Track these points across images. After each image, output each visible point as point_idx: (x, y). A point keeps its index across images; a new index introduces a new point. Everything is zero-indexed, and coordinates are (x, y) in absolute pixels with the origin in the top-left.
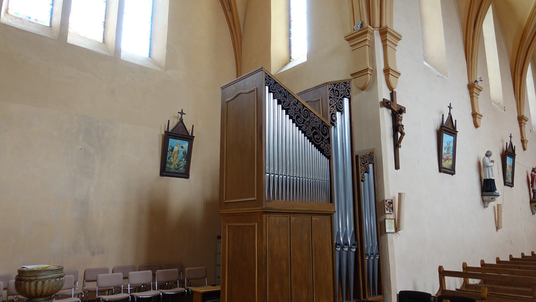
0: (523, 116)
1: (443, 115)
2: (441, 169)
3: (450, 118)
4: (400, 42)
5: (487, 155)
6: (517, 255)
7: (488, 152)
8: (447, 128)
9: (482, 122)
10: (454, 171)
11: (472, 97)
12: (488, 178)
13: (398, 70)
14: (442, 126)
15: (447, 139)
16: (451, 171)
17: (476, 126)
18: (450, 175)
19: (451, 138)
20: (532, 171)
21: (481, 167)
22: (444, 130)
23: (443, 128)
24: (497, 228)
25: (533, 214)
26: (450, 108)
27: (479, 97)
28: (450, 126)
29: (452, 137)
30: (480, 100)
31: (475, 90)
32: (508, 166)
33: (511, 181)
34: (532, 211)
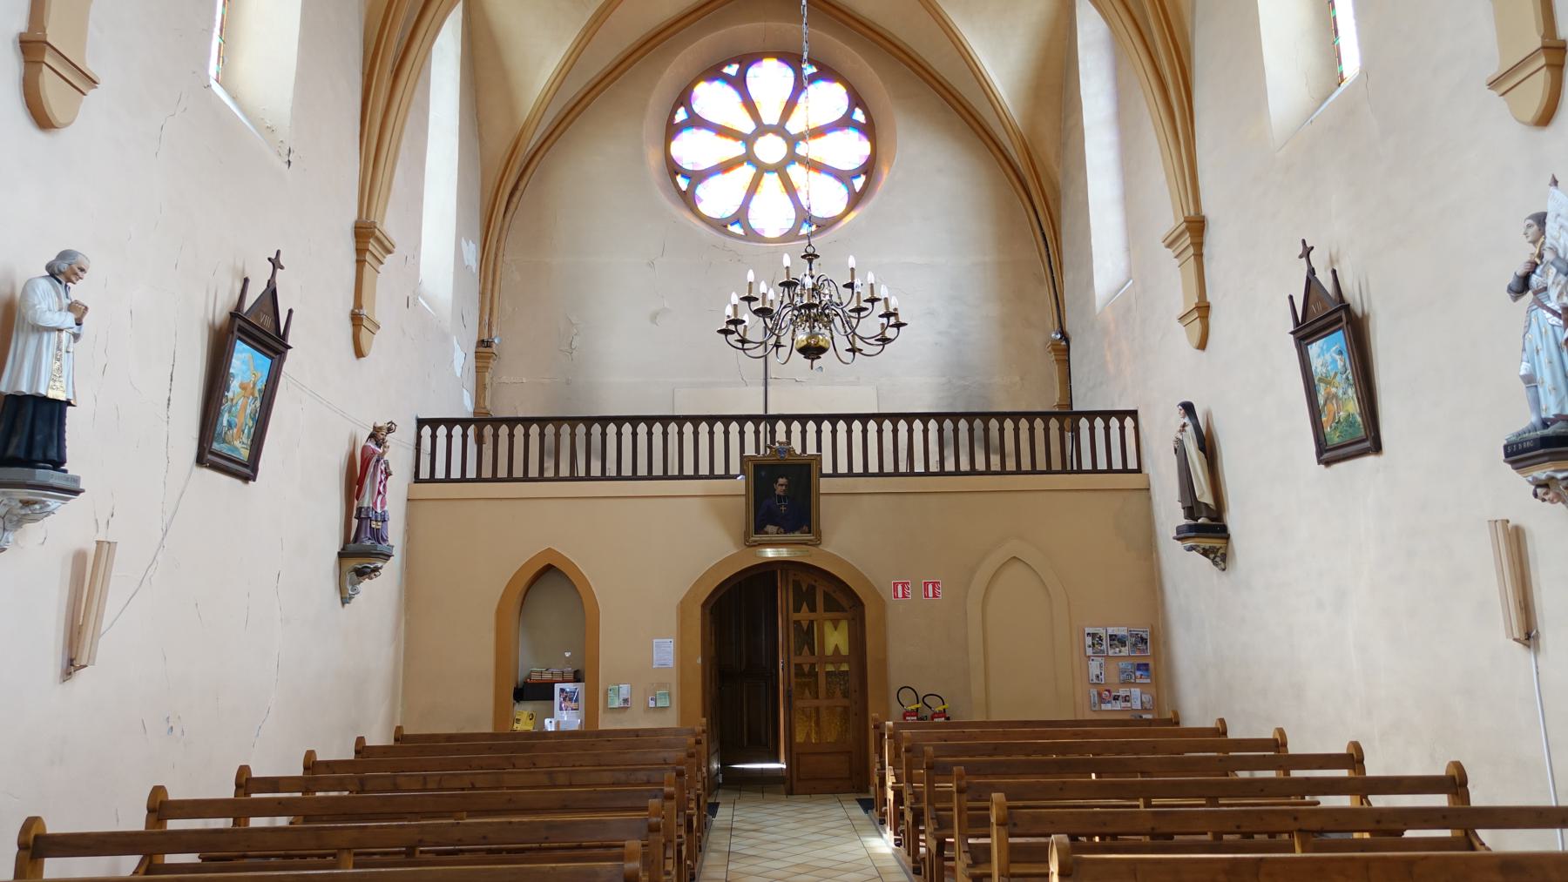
0: (373, 226)
1: (246, 280)
2: (207, 456)
3: (271, 293)
4: (389, 256)
5: (53, 273)
6: (338, 749)
7: (64, 255)
8: (255, 327)
9: (377, 345)
10: (255, 469)
11: (360, 262)
12: (24, 388)
13: (90, 67)
14: (235, 315)
15: (245, 363)
16: (246, 471)
17: (359, 353)
18: (238, 482)
19: (265, 363)
20: (372, 436)
21: (360, 473)
22: (241, 330)
23: (238, 322)
24: (71, 666)
25: (345, 600)
26: (276, 263)
27: (381, 268)
28: (266, 322)
29: (269, 361)
30: (386, 279)
31: (373, 246)
32: (235, 385)
33: (244, 454)
34: (342, 589)
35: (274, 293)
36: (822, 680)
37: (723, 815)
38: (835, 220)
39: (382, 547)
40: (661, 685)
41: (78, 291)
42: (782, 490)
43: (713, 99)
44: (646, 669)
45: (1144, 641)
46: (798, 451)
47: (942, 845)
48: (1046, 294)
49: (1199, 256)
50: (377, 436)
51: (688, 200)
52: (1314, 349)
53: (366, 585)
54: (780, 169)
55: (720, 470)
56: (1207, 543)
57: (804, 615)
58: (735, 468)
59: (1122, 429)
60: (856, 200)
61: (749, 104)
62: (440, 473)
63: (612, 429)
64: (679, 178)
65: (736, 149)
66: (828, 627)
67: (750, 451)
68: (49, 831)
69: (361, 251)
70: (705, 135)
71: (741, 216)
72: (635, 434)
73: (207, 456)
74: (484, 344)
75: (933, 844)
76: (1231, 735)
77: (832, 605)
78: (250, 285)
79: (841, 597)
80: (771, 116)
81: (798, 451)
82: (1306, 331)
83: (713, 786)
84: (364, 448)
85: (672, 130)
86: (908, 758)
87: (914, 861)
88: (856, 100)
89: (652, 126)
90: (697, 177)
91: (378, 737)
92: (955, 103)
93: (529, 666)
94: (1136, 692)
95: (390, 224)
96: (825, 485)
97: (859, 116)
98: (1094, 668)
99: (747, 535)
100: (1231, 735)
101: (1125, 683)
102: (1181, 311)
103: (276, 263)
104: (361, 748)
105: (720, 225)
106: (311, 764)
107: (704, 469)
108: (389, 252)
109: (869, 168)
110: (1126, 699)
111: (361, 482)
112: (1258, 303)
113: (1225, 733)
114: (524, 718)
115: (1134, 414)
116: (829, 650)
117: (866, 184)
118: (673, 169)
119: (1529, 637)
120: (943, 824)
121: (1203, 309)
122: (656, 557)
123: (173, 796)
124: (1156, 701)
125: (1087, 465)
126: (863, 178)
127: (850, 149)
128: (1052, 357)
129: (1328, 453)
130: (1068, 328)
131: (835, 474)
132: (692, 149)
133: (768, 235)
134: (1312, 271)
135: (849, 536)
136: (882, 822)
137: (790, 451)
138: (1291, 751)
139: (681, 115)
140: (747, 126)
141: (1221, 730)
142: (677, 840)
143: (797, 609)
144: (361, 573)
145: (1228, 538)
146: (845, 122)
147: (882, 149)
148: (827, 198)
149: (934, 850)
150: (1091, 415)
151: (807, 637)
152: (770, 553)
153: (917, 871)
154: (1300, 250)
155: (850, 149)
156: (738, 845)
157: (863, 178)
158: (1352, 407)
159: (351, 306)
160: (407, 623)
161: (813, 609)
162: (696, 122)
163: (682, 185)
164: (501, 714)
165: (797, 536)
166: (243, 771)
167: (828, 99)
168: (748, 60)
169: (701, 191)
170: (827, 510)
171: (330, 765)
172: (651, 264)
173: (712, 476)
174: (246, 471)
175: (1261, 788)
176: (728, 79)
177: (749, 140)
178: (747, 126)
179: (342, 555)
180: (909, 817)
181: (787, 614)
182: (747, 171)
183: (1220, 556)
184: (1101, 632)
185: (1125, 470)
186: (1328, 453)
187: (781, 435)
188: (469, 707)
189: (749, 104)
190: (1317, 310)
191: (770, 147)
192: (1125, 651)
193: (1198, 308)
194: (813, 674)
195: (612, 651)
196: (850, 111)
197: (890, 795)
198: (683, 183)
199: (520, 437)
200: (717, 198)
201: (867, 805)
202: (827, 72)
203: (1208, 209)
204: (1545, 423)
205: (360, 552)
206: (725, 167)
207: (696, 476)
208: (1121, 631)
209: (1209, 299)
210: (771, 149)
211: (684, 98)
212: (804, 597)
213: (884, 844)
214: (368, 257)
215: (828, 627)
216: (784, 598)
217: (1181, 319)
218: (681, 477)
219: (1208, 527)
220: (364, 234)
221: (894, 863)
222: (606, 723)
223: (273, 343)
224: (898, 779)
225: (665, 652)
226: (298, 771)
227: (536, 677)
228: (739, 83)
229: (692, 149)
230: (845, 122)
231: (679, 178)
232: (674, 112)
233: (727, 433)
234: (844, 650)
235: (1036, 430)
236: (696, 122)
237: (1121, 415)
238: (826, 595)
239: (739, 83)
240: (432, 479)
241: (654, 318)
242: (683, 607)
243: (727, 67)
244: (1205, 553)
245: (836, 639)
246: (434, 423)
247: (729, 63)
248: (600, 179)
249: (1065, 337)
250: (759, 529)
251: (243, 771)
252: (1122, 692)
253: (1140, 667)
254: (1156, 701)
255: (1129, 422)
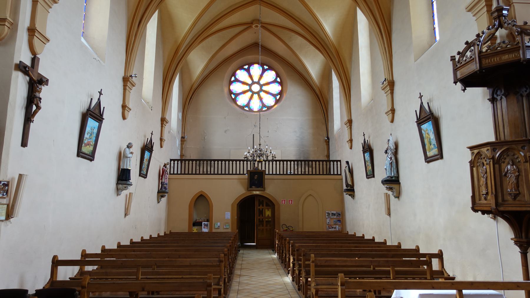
0: (165, 118)
1: (92, 99)
2: (80, 154)
3: (99, 104)
5: (128, 147)
8: (94, 113)
11: (125, 89)
13: (48, 36)
14: (89, 110)
15: (92, 124)
16: (91, 157)
18: (89, 161)
20: (164, 166)
22: (90, 114)
24: (126, 215)
26: (100, 93)
28: (97, 112)
30: (132, 94)
35: (100, 102)
36: (265, 222)
37: (241, 252)
38: (272, 107)
39: (167, 191)
40: (227, 223)
41: (131, 150)
42: (256, 178)
43: (241, 75)
44: (224, 218)
45: (340, 215)
46: (260, 169)
47: (307, 280)
48: (324, 127)
49: (392, 93)
50: (165, 166)
51: (235, 101)
52: (424, 127)
53: (163, 199)
54: (258, 93)
55: (242, 173)
56: (350, 193)
57: (261, 207)
58: (245, 172)
59: (337, 164)
60: (277, 102)
61: (250, 76)
62: (176, 172)
63: (216, 162)
64: (232, 95)
65: (247, 88)
66: (266, 210)
67: (249, 169)
68: (59, 259)
69: (125, 86)
70: (239, 84)
71: (248, 105)
72: (222, 164)
73: (80, 154)
74: (183, 138)
75: (304, 280)
76: (376, 241)
77: (267, 205)
78: (93, 100)
79: (270, 203)
80: (256, 79)
81: (260, 169)
82: (420, 122)
83: (239, 247)
84: (163, 169)
85: (231, 83)
86: (281, 238)
87: (299, 286)
88: (278, 75)
89: (226, 82)
90: (237, 95)
91: (162, 234)
92: (302, 77)
93: (196, 217)
94: (337, 226)
95: (167, 117)
96: (266, 177)
97: (278, 80)
98: (328, 221)
99: (248, 188)
100: (376, 241)
101: (335, 224)
102: (386, 111)
103: (100, 93)
104: (132, 242)
105: (242, 107)
106: (103, 249)
107: (238, 173)
108: (134, 86)
109: (281, 93)
110: (335, 228)
111: (162, 176)
112: (408, 112)
113: (400, 247)
114: (195, 230)
115: (340, 161)
116: (267, 215)
117: (280, 98)
118: (231, 92)
119: (389, 214)
120: (308, 274)
121: (393, 111)
122: (226, 194)
123: (60, 258)
124: (342, 228)
125: (332, 173)
126: (279, 96)
127: (276, 88)
128: (325, 143)
129: (428, 160)
130: (329, 136)
131: (269, 174)
132: (236, 88)
133: (255, 110)
134: (422, 103)
135: (271, 189)
136: (289, 273)
137: (258, 169)
138: (402, 248)
139: (233, 79)
140: (250, 82)
141: (385, 243)
142: (224, 277)
143: (259, 206)
144: (162, 196)
145: (354, 192)
146: (275, 81)
147: (284, 89)
148: (269, 101)
149: (304, 282)
150: (334, 161)
151: (261, 212)
152: (255, 193)
153: (299, 290)
154: (419, 96)
155: (276, 88)
156: (243, 279)
157: (279, 96)
158: (370, 168)
159: (121, 103)
160: (168, 208)
161: (263, 206)
162: (237, 80)
163: (233, 97)
164: (190, 228)
165: (260, 189)
166: (84, 251)
167: (270, 75)
168: (251, 64)
169: (238, 98)
170: (267, 182)
171: (110, 250)
172: (225, 118)
173: (240, 174)
174: (91, 157)
175: (410, 263)
176: (245, 69)
177: (250, 86)
178: (250, 82)
179: (158, 193)
180: (297, 272)
181: (257, 207)
182: (249, 94)
183: (353, 196)
184: (330, 212)
185: (337, 174)
186: (428, 160)
187: (256, 165)
188: (183, 227)
189: (250, 76)
190: (423, 115)
191: (255, 86)
192: (335, 217)
193: (391, 110)
194: (263, 221)
195: (216, 214)
196: (276, 79)
197: (291, 265)
198: (233, 96)
199: (194, 163)
200: (242, 100)
201: (273, 250)
202: (271, 68)
203: (353, 118)
204: (392, 177)
205: (162, 192)
206: (244, 92)
207: (236, 174)
208: (334, 212)
209: (395, 107)
210: (256, 88)
211: (234, 74)
212: (261, 203)
213: (288, 279)
214: (127, 88)
215: (266, 210)
216: (257, 203)
217: (386, 113)
218: (232, 174)
219: (351, 190)
220: (126, 80)
221: (291, 284)
222: (214, 231)
223: (99, 117)
224: (294, 259)
225: (228, 215)
226: (100, 252)
227: (198, 221)
228: (248, 70)
229: (236, 88)
230: (275, 81)
231: (232, 95)
232: (231, 78)
233: (243, 164)
234: (270, 215)
235: (318, 164)
236: (237, 80)
237: (337, 161)
238: (266, 203)
239: (248, 70)
240: (174, 174)
241: (225, 131)
242: (233, 205)
243: (246, 66)
244: (350, 195)
245: (268, 213)
246: (174, 160)
247: (245, 65)
248: (212, 94)
249: (328, 138)
250: (251, 187)
251: (84, 251)
252: (334, 226)
253: (338, 221)
254: (342, 228)
255: (339, 163)
